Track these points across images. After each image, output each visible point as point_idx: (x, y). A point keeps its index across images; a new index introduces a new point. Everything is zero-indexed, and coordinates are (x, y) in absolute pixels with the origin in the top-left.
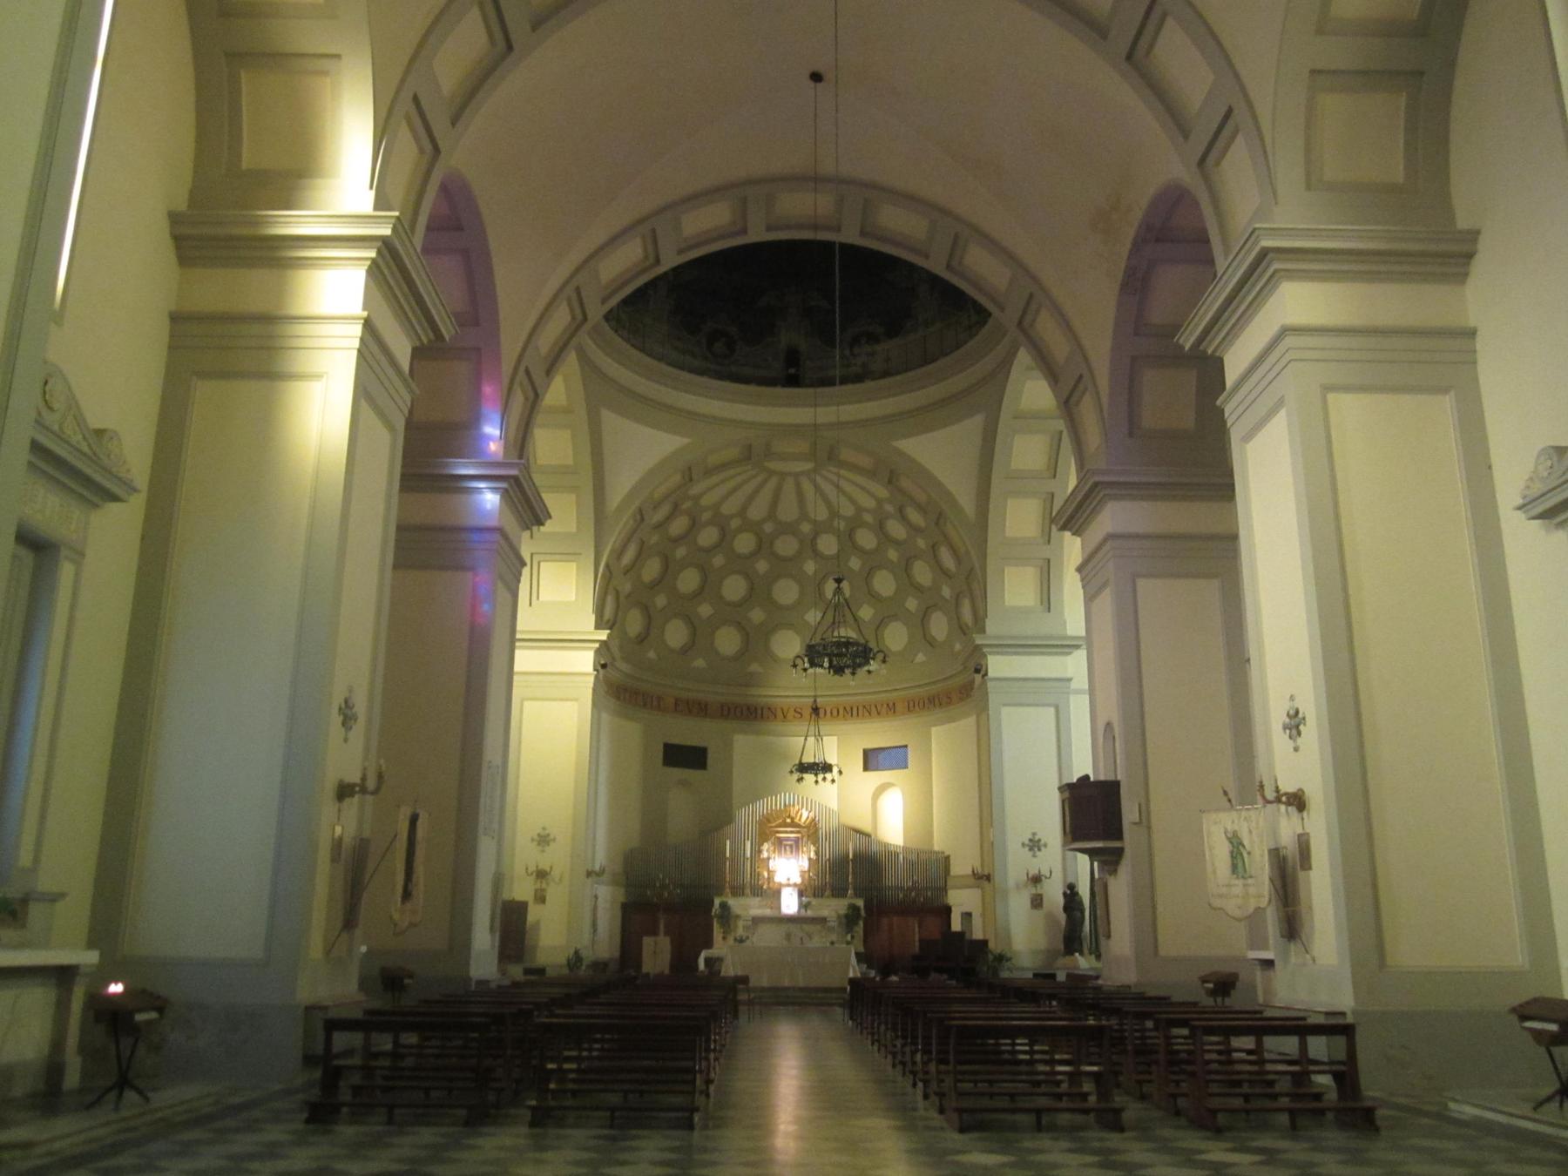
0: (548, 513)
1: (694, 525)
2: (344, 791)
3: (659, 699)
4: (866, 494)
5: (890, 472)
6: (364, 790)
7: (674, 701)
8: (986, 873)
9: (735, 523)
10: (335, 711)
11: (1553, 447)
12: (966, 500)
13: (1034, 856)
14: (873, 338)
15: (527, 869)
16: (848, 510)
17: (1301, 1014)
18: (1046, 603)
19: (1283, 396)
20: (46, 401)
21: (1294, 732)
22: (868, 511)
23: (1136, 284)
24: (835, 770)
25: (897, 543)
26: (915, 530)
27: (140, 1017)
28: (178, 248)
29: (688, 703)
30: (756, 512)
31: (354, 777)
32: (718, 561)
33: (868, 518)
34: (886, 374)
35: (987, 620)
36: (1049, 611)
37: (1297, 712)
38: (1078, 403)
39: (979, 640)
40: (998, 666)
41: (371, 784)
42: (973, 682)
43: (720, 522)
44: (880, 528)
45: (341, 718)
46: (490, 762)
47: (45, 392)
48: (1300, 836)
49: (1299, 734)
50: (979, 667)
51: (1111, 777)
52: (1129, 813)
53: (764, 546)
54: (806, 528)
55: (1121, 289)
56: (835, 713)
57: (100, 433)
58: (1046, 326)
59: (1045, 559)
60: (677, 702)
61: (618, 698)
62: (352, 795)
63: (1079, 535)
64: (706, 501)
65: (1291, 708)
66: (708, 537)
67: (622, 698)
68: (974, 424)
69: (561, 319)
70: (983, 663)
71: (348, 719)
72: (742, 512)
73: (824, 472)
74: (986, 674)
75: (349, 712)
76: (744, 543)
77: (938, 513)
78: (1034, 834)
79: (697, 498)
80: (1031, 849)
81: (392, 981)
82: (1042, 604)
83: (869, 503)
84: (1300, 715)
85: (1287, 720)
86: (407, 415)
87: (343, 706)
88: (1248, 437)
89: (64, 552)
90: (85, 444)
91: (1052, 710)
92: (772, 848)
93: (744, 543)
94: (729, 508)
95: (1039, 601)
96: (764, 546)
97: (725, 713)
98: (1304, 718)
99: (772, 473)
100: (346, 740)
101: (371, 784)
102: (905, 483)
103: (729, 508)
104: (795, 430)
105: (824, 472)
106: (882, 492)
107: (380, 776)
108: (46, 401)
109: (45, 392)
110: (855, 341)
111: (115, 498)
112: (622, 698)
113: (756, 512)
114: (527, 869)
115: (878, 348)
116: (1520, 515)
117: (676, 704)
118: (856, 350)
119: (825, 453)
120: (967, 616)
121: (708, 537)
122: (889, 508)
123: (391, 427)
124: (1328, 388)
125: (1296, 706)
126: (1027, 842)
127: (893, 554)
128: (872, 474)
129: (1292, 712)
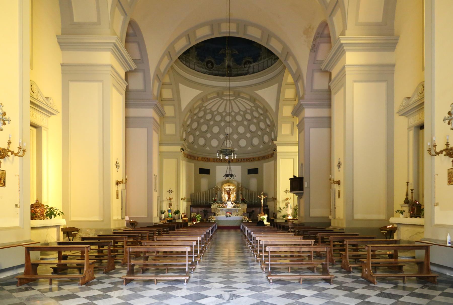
0: (165, 113)
1: (205, 114)
2: (118, 183)
3: (198, 157)
4: (249, 105)
5: (253, 99)
6: (123, 183)
7: (201, 158)
8: (275, 198)
9: (215, 113)
10: (114, 165)
11: (406, 97)
12: (273, 107)
13: (287, 194)
14: (250, 63)
15: (167, 198)
16: (244, 109)
17: (333, 229)
18: (292, 133)
19: (60, 216)
20: (32, 91)
21: (339, 167)
22: (248, 109)
23: (314, 49)
24: (234, 176)
25: (256, 118)
26: (254, 117)
27: (73, 233)
28: (60, 46)
29: (205, 158)
30: (221, 110)
31: (120, 180)
32: (212, 123)
33: (249, 111)
34: (254, 73)
35: (277, 138)
36: (293, 135)
37: (340, 162)
38: (206, 130)
39: (275, 142)
40: (279, 149)
41: (124, 181)
42: (274, 153)
43: (212, 113)
44: (252, 114)
45: (116, 166)
46: (154, 174)
47: (31, 89)
48: (338, 190)
49: (340, 167)
50: (275, 150)
51: (302, 177)
52: (306, 185)
53: (223, 119)
54: (233, 114)
55: (311, 51)
56: (241, 160)
57: (47, 98)
58: (290, 62)
59: (292, 122)
60: (202, 158)
61: (187, 158)
62: (120, 183)
63: (298, 117)
64: (208, 107)
65: (339, 161)
66: (209, 117)
67: (188, 158)
68: (276, 86)
69: (166, 61)
70: (276, 148)
71: (117, 165)
72: (217, 110)
73: (237, 99)
74: (277, 151)
75: (118, 165)
76: (218, 118)
77: (266, 110)
78: (287, 189)
79: (205, 107)
80: (286, 192)
81: (132, 224)
82: (291, 133)
83: (249, 107)
84: (340, 163)
85: (338, 164)
86: (125, 90)
87: (116, 163)
88: (335, 94)
89: (43, 128)
90: (44, 101)
91: (292, 160)
92: (225, 193)
93: (218, 118)
94: (214, 109)
95: (291, 133)
96: (223, 119)
97: (214, 161)
98: (341, 164)
99: (224, 100)
100: (117, 171)
101: (124, 181)
102: (257, 102)
103: (214, 109)
104: (230, 89)
105: (237, 99)
106: (252, 105)
107: (126, 179)
108: (32, 91)
109: (31, 89)
110: (245, 64)
111: (53, 114)
112: (188, 158)
113: (221, 110)
114: (167, 198)
115: (252, 65)
116: (397, 114)
117: (202, 159)
118: (245, 66)
119: (237, 95)
120: (273, 137)
121: (209, 117)
122: (254, 109)
123: (122, 94)
124: (355, 81)
125: (340, 161)
126: (285, 191)
127: (255, 121)
128: (250, 100)
129: (339, 163)
